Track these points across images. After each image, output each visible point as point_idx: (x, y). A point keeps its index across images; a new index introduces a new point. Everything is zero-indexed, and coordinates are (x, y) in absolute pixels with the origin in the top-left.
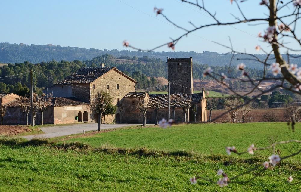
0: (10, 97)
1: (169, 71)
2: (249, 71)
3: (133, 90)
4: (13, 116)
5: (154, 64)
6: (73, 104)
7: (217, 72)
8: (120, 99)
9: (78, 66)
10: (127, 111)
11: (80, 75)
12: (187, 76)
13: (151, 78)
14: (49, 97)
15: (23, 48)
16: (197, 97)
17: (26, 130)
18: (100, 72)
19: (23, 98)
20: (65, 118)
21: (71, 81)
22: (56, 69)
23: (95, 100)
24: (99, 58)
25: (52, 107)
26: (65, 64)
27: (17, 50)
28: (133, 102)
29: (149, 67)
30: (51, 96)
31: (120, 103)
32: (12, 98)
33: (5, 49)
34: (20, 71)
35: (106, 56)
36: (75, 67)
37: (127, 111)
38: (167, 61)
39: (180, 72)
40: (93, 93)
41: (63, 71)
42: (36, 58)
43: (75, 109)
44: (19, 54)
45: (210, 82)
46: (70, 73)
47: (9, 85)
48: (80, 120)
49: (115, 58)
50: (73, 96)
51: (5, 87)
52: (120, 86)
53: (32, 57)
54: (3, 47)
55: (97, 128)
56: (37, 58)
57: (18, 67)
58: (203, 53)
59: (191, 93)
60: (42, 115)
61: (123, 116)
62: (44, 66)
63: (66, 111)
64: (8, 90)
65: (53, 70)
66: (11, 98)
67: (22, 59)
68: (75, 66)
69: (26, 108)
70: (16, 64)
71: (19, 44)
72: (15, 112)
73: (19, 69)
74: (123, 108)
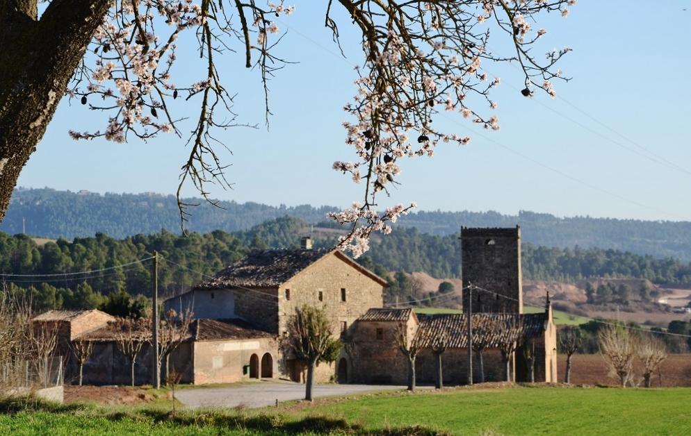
0: (90, 318)
1: (466, 258)
2: (632, 261)
3: (379, 304)
4: (95, 363)
5: (401, 242)
6: (240, 336)
7: (555, 262)
8: (349, 325)
9: (222, 244)
10: (365, 353)
11: (253, 267)
12: (508, 270)
13: (397, 273)
14: (184, 317)
15: (87, 202)
16: (534, 323)
17: (142, 397)
18: (300, 259)
19: (124, 320)
20: (219, 369)
21: (233, 280)
22: (169, 251)
23: (288, 325)
24: (268, 226)
25: (191, 341)
26: (191, 238)
27: (72, 206)
28: (380, 332)
29: (390, 246)
30: (188, 315)
31: (349, 333)
32: (95, 320)
33: (45, 205)
34: (85, 256)
35: (287, 220)
36: (215, 246)
37: (365, 353)
38: (459, 234)
39: (492, 261)
40: (285, 310)
41: (187, 256)
42: (118, 225)
43: (244, 349)
44: (76, 215)
45: (538, 286)
46: (204, 260)
47: (61, 289)
48: (254, 375)
49: (306, 226)
50: (237, 317)
51: (54, 293)
52: (347, 292)
53: (108, 221)
54: (40, 198)
55: (303, 395)
56: (120, 226)
57: (82, 247)
58: (518, 215)
59: (517, 311)
60: (166, 361)
61: (354, 365)
62: (141, 244)
63: (222, 353)
64: (61, 302)
65: (163, 253)
66: (92, 322)
67: (84, 227)
68: (215, 243)
69: (130, 345)
70: (76, 240)
71: (76, 193)
72: (101, 353)
73: (81, 251)
74: (356, 347)
